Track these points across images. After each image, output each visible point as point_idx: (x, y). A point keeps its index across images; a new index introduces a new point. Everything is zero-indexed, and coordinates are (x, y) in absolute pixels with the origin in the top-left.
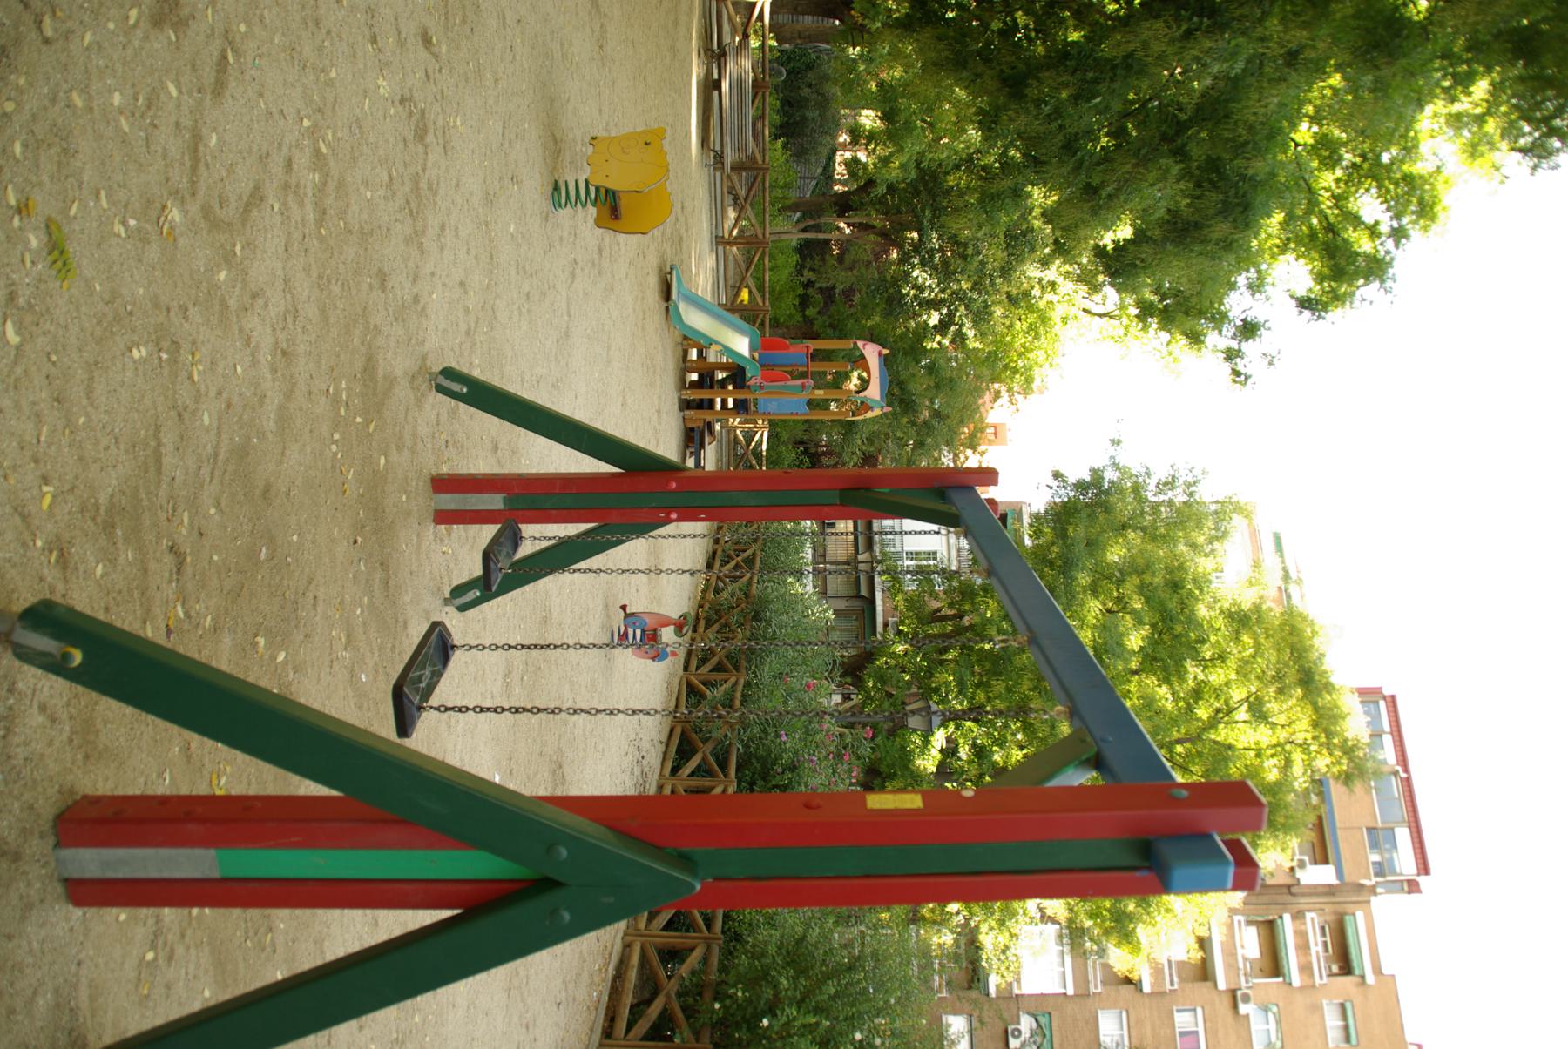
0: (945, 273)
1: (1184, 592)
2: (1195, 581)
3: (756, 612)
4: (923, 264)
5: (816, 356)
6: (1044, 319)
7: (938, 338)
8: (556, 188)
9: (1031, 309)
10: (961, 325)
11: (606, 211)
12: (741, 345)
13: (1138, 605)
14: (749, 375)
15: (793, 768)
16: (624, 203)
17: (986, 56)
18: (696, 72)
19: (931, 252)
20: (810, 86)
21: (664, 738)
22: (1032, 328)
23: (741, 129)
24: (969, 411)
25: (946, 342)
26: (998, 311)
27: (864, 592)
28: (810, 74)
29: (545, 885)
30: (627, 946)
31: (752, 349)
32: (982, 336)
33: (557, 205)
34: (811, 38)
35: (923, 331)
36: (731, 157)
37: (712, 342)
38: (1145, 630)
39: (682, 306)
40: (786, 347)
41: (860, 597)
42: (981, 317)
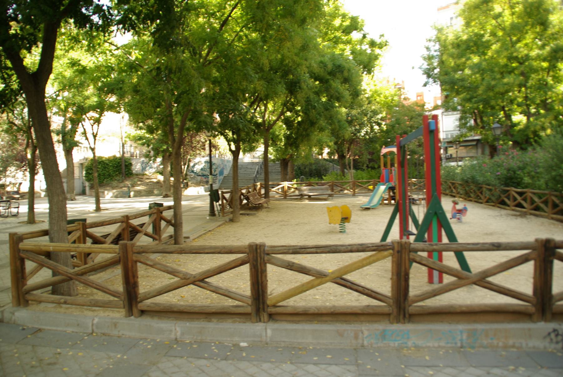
0: (362, 125)
1: (460, 43)
2: (457, 39)
3: (466, 182)
4: (359, 132)
5: (385, 165)
6: (376, 92)
7: (382, 126)
8: (341, 232)
9: (372, 96)
10: (378, 119)
11: (346, 220)
12: (382, 188)
13: (464, 59)
14: (391, 186)
15: (509, 170)
16: (344, 216)
17: (306, 130)
18: (307, 202)
19: (356, 130)
20: (305, 168)
21: (499, 209)
22: (379, 95)
23: (322, 189)
24: (409, 109)
25: (384, 123)
26: (373, 107)
27: (474, 143)
28: (302, 168)
29: (436, 213)
30: (552, 219)
31: (384, 185)
32: (381, 113)
33: (344, 232)
34: (293, 169)
35: (382, 131)
36: (329, 192)
37: (381, 197)
38: (472, 56)
39: (372, 205)
40: (383, 176)
41: (476, 145)
42: (375, 113)
